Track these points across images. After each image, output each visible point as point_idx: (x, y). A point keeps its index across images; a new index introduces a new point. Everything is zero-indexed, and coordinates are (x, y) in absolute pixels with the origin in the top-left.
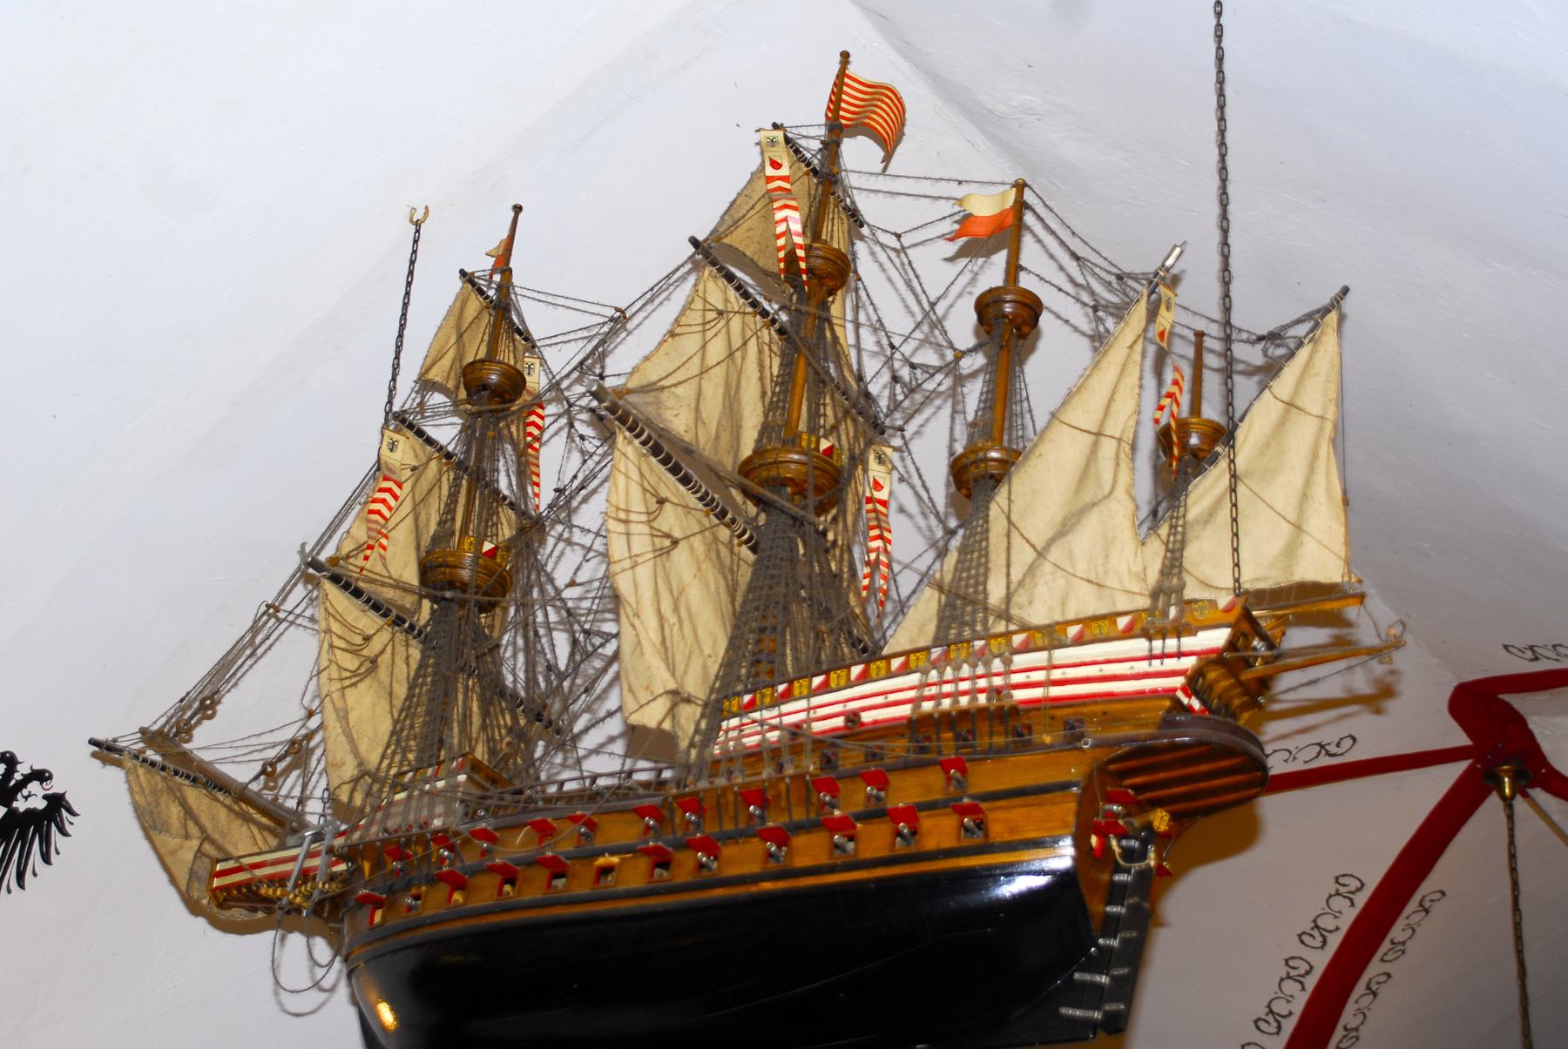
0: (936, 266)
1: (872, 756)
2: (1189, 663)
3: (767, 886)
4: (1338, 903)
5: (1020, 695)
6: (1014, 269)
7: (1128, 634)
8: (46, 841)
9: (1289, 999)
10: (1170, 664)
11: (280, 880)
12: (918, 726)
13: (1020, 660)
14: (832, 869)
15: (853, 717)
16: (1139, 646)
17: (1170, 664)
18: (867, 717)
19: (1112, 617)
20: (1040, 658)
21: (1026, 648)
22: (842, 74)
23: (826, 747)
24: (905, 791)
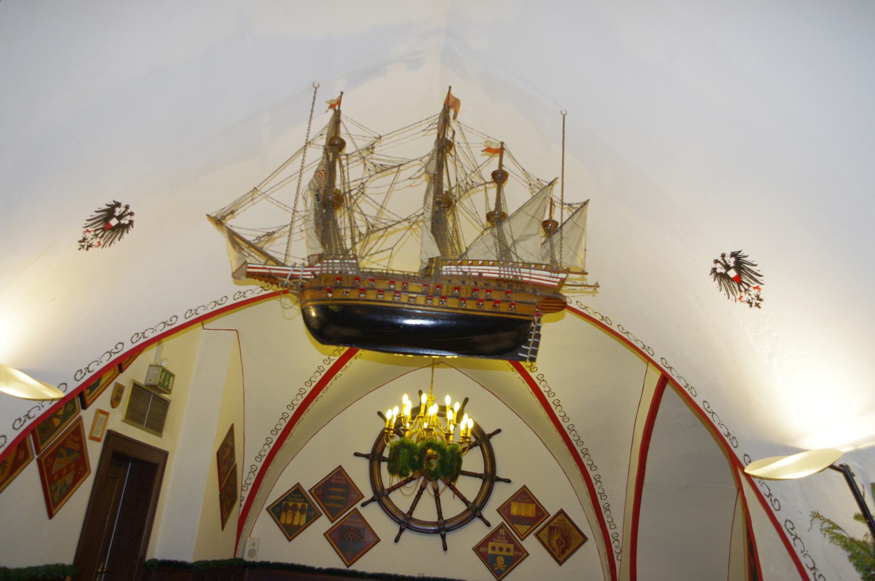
0: (481, 158)
1: (486, 285)
2: (558, 280)
3: (460, 312)
4: (317, 374)
5: (524, 279)
6: (501, 165)
7: (545, 270)
8: (122, 234)
9: (265, 451)
10: (555, 280)
11: (285, 276)
12: (498, 280)
13: (522, 270)
14: (457, 309)
15: (480, 274)
16: (548, 274)
17: (555, 280)
18: (484, 275)
19: (541, 265)
20: (528, 271)
21: (522, 267)
22: (449, 93)
23: (471, 277)
24: (496, 296)
